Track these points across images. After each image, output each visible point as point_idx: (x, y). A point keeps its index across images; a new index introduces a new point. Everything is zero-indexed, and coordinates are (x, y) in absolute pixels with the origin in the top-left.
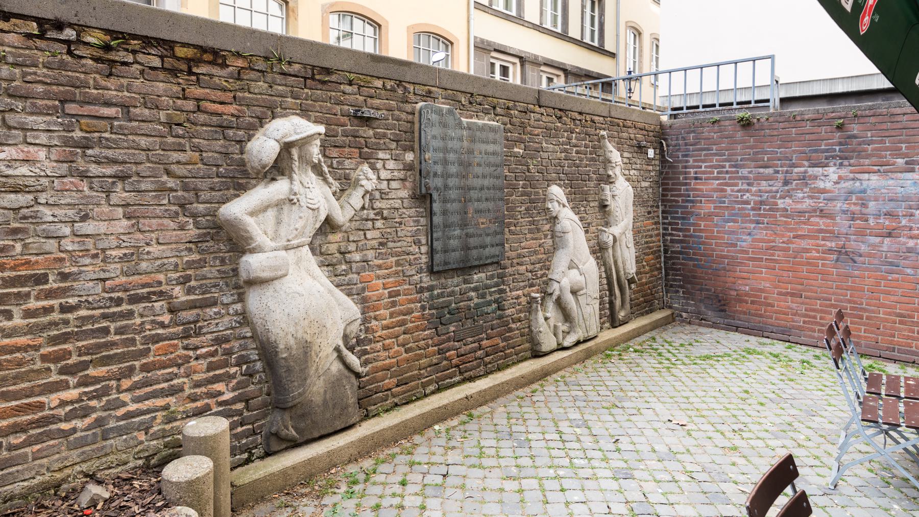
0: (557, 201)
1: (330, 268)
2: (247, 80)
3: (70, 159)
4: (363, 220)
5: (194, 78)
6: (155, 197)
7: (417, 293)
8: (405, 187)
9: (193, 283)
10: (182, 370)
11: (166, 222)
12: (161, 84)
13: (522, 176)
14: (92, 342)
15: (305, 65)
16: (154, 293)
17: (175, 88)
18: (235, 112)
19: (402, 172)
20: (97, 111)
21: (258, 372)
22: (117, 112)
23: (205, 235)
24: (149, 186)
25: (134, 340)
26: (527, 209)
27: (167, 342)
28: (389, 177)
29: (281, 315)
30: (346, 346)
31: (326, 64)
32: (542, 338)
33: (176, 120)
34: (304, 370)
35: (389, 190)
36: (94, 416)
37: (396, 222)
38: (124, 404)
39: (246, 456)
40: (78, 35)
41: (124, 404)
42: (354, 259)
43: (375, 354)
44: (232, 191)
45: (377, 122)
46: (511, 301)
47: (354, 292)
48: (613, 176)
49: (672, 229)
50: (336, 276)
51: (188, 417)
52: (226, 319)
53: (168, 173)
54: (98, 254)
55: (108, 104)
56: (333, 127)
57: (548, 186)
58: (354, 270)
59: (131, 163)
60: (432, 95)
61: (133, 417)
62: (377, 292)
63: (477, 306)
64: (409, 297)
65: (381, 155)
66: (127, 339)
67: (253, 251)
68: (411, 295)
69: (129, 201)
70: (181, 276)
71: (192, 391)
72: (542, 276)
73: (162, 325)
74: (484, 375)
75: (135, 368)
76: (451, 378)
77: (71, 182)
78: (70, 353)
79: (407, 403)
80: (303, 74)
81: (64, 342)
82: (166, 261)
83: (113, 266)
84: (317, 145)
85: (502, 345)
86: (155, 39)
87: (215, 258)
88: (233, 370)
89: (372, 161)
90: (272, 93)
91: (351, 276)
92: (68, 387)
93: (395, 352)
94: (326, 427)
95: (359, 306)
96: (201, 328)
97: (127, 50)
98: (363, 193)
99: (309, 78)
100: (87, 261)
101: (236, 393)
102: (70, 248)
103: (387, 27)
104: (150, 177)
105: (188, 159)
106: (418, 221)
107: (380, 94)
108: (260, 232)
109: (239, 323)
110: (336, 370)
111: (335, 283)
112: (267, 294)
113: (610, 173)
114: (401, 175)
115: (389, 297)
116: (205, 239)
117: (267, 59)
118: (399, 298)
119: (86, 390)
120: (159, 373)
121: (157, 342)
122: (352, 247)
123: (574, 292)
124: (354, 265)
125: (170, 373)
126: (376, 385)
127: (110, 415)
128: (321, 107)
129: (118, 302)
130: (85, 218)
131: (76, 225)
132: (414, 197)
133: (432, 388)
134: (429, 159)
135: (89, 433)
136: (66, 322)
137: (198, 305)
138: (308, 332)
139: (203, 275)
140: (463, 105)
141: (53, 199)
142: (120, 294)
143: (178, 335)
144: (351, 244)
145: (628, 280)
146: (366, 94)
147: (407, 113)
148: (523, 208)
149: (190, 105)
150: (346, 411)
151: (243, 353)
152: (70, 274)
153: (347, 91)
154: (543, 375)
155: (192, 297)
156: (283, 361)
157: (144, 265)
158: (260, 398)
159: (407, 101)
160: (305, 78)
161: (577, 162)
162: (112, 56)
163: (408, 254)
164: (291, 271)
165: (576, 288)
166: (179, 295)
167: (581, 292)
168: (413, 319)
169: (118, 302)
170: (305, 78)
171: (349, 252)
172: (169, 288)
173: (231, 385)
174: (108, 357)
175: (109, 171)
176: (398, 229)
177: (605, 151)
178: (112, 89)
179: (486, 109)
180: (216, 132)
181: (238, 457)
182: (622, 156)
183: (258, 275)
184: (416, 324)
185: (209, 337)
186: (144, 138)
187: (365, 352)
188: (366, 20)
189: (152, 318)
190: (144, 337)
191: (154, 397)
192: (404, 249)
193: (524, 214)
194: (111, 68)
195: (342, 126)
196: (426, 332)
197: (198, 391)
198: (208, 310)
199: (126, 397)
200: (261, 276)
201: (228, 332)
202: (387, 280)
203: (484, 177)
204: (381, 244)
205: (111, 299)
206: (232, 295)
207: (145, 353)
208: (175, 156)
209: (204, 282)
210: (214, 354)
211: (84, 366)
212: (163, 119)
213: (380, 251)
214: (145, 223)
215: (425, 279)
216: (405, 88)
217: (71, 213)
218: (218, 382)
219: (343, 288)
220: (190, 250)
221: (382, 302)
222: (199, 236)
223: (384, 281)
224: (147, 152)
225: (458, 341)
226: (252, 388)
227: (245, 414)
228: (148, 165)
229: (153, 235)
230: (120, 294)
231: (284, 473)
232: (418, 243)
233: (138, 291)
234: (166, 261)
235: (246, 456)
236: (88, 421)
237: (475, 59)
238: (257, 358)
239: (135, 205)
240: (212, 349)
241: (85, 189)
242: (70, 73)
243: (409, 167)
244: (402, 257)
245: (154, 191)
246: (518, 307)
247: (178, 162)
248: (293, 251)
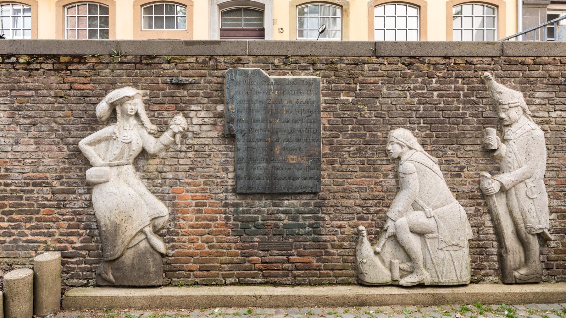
0: (398, 143)
2: (99, 69)
3: (12, 116)
4: (177, 151)
5: (69, 72)
6: (48, 134)
7: (223, 207)
8: (216, 130)
9: (64, 180)
10: (55, 225)
11: (53, 147)
12: (53, 77)
14: (15, 202)
15: (135, 56)
16: (44, 183)
17: (59, 79)
18: (91, 88)
19: (212, 119)
20: (24, 93)
21: (96, 236)
22: (32, 93)
23: (72, 155)
24: (46, 129)
25: (33, 205)
27: (49, 209)
28: (200, 122)
29: (102, 205)
31: (150, 53)
32: (366, 269)
33: (59, 94)
34: (114, 240)
35: (200, 132)
36: (14, 237)
37: (206, 154)
38: (27, 235)
39: (85, 282)
40: (17, 59)
41: (27, 235)
42: (167, 177)
43: (181, 244)
44: (89, 132)
45: (190, 86)
46: (331, 229)
47: (166, 198)
48: (507, 118)
50: (153, 186)
51: (55, 250)
52: (80, 202)
53: (56, 123)
54: (21, 160)
55: (28, 90)
56: (155, 91)
57: (391, 129)
58: (167, 184)
60: (242, 62)
61: (30, 243)
62: (186, 201)
63: (286, 226)
64: (215, 209)
65: (193, 107)
66: (30, 203)
68: (217, 207)
70: (58, 176)
71: (60, 237)
72: (377, 212)
73: (46, 199)
74: (289, 285)
75: (33, 219)
76: (254, 278)
77: (13, 127)
78: (6, 205)
79: (207, 285)
80: (134, 61)
81: (4, 200)
82: (51, 167)
83: (27, 167)
85: (315, 264)
86: (49, 55)
87: (76, 168)
88: (81, 231)
89: (185, 112)
90: (113, 75)
91: (164, 188)
92: (4, 221)
93: (198, 246)
94: (132, 281)
95: (170, 208)
96: (66, 204)
97: (37, 63)
99: (138, 63)
100: (16, 163)
101: (82, 245)
102: (10, 157)
103: (426, 7)
104: (46, 124)
106: (227, 155)
107: (193, 66)
108: (96, 155)
109: (87, 205)
110: (144, 246)
111: (152, 191)
112: (97, 191)
113: (503, 115)
114: (212, 121)
115: (196, 206)
116: (72, 157)
117: (110, 55)
118: (205, 208)
119: (11, 224)
120: (44, 223)
121: (44, 208)
122: (166, 169)
124: (168, 181)
125: (48, 225)
126: (181, 264)
127: (20, 239)
128: (146, 79)
129: (28, 184)
130: (17, 143)
131: (14, 146)
132: (223, 136)
133: (231, 280)
134: (232, 109)
135: (11, 245)
136: (6, 191)
137: (65, 192)
138: (118, 218)
139: (69, 176)
140: (276, 66)
141: (5, 134)
142: (29, 181)
143: (54, 206)
144: (167, 167)
146: (181, 68)
147: (218, 77)
149: (66, 86)
150: (148, 275)
151: (88, 223)
152: (9, 169)
153: (166, 68)
154: (360, 303)
155: (63, 187)
156: (103, 232)
157: (41, 168)
158: (96, 251)
159: (217, 69)
160: (135, 63)
162: (31, 67)
163: (216, 177)
164: (112, 179)
166: (56, 185)
167: (431, 235)
168: (217, 225)
169: (28, 184)
170: (135, 63)
171: (165, 172)
172: (51, 181)
173: (80, 239)
174: (21, 210)
175: (28, 121)
176: (208, 159)
177: (492, 93)
178: (30, 82)
179: (303, 66)
180: (80, 99)
181: (81, 281)
184: (220, 229)
185: (70, 210)
186: (44, 105)
187: (173, 240)
188: (408, 5)
189: (42, 195)
190: (38, 204)
191: (41, 235)
192: (211, 173)
193: (353, 154)
194: (29, 71)
195: (162, 90)
196: (229, 237)
197: (62, 238)
198: (71, 195)
199: (28, 232)
201: (81, 209)
202: (195, 194)
203: (295, 121)
204: (191, 168)
205: (25, 183)
206: (84, 189)
207: (38, 212)
208: (58, 113)
209: (70, 180)
210: (72, 220)
211: (11, 213)
212: (53, 95)
213: (190, 173)
214: (43, 147)
215: (230, 198)
216: (216, 59)
217: (11, 141)
218: (74, 236)
219: (158, 194)
220: (64, 162)
221: (190, 208)
222: (69, 155)
223: (193, 194)
225: (262, 250)
226: (93, 244)
227: (87, 258)
228: (47, 118)
229: (46, 153)
230: (29, 181)
231: (94, 299)
232: (227, 171)
233: (37, 181)
234: (51, 167)
235: (85, 282)
236: (11, 239)
237: (523, 15)
238: (96, 227)
239: (38, 138)
240: (71, 217)
241: (18, 130)
242: (14, 77)
243: (220, 115)
244: (210, 179)
245: (49, 131)
246: (340, 235)
247: (60, 116)
248: (116, 168)
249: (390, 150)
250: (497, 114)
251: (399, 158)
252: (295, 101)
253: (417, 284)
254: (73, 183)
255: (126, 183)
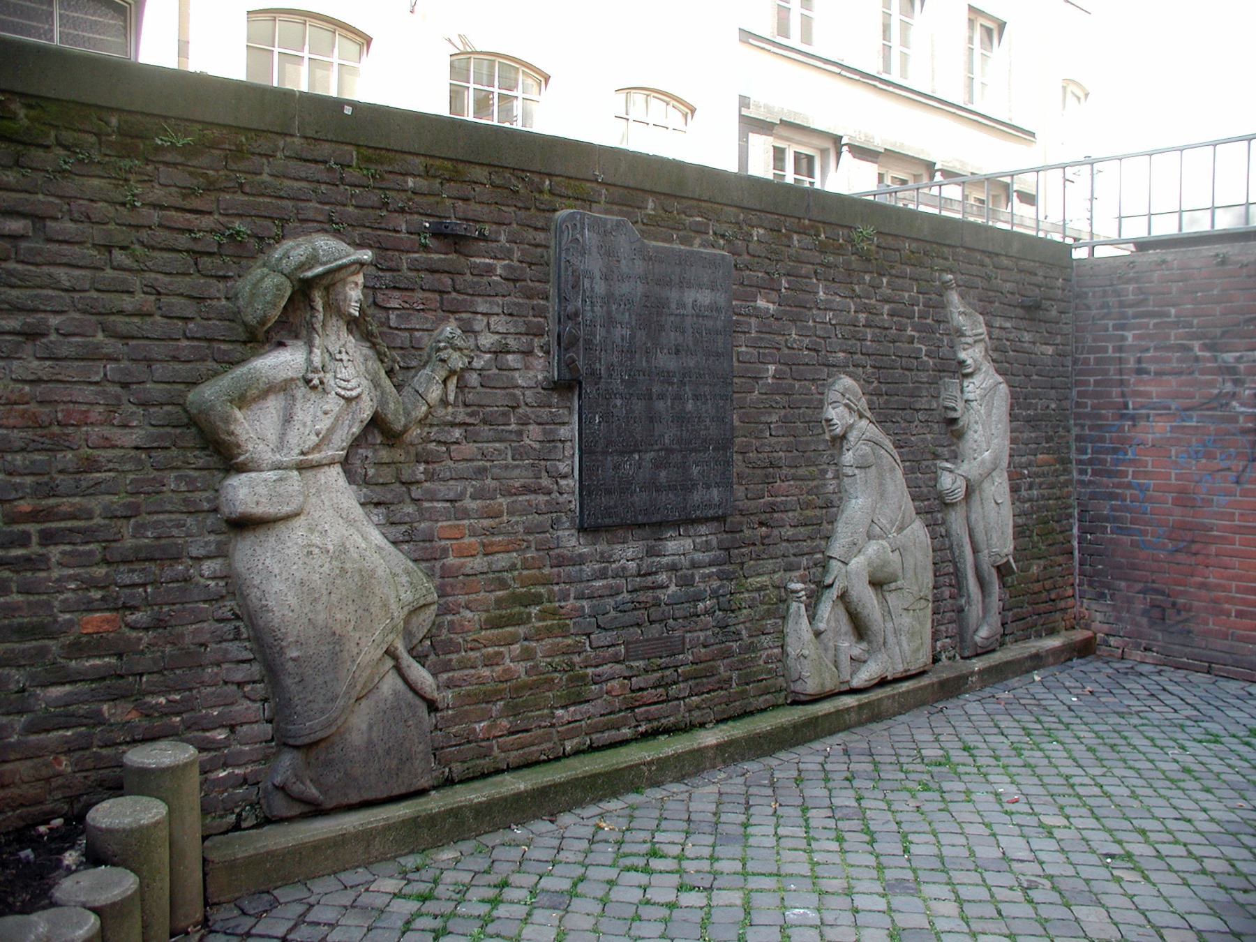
1: (382, 510)
13: (771, 355)
19: (524, 339)
26: (784, 420)
30: (410, 651)
39: (232, 818)
49: (1094, 473)
59: (45, 311)
67: (242, 469)
69: (40, 374)
84: (356, 284)
89: (464, 315)
98: (444, 374)
105: (138, 307)
116: (162, 445)
123: (877, 584)
145: (998, 568)
148: (774, 418)
150: (408, 764)
161: (894, 331)
165: (880, 576)
167: (893, 586)
182: (989, 325)
183: (249, 510)
200: (254, 511)
224: (72, 294)
249: (832, 420)
250: (955, 353)
251: (844, 437)
252: (690, 305)
253: (877, 680)
254: (173, 526)
255: (341, 516)
